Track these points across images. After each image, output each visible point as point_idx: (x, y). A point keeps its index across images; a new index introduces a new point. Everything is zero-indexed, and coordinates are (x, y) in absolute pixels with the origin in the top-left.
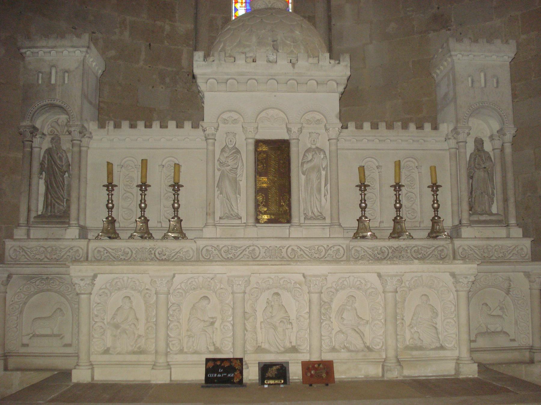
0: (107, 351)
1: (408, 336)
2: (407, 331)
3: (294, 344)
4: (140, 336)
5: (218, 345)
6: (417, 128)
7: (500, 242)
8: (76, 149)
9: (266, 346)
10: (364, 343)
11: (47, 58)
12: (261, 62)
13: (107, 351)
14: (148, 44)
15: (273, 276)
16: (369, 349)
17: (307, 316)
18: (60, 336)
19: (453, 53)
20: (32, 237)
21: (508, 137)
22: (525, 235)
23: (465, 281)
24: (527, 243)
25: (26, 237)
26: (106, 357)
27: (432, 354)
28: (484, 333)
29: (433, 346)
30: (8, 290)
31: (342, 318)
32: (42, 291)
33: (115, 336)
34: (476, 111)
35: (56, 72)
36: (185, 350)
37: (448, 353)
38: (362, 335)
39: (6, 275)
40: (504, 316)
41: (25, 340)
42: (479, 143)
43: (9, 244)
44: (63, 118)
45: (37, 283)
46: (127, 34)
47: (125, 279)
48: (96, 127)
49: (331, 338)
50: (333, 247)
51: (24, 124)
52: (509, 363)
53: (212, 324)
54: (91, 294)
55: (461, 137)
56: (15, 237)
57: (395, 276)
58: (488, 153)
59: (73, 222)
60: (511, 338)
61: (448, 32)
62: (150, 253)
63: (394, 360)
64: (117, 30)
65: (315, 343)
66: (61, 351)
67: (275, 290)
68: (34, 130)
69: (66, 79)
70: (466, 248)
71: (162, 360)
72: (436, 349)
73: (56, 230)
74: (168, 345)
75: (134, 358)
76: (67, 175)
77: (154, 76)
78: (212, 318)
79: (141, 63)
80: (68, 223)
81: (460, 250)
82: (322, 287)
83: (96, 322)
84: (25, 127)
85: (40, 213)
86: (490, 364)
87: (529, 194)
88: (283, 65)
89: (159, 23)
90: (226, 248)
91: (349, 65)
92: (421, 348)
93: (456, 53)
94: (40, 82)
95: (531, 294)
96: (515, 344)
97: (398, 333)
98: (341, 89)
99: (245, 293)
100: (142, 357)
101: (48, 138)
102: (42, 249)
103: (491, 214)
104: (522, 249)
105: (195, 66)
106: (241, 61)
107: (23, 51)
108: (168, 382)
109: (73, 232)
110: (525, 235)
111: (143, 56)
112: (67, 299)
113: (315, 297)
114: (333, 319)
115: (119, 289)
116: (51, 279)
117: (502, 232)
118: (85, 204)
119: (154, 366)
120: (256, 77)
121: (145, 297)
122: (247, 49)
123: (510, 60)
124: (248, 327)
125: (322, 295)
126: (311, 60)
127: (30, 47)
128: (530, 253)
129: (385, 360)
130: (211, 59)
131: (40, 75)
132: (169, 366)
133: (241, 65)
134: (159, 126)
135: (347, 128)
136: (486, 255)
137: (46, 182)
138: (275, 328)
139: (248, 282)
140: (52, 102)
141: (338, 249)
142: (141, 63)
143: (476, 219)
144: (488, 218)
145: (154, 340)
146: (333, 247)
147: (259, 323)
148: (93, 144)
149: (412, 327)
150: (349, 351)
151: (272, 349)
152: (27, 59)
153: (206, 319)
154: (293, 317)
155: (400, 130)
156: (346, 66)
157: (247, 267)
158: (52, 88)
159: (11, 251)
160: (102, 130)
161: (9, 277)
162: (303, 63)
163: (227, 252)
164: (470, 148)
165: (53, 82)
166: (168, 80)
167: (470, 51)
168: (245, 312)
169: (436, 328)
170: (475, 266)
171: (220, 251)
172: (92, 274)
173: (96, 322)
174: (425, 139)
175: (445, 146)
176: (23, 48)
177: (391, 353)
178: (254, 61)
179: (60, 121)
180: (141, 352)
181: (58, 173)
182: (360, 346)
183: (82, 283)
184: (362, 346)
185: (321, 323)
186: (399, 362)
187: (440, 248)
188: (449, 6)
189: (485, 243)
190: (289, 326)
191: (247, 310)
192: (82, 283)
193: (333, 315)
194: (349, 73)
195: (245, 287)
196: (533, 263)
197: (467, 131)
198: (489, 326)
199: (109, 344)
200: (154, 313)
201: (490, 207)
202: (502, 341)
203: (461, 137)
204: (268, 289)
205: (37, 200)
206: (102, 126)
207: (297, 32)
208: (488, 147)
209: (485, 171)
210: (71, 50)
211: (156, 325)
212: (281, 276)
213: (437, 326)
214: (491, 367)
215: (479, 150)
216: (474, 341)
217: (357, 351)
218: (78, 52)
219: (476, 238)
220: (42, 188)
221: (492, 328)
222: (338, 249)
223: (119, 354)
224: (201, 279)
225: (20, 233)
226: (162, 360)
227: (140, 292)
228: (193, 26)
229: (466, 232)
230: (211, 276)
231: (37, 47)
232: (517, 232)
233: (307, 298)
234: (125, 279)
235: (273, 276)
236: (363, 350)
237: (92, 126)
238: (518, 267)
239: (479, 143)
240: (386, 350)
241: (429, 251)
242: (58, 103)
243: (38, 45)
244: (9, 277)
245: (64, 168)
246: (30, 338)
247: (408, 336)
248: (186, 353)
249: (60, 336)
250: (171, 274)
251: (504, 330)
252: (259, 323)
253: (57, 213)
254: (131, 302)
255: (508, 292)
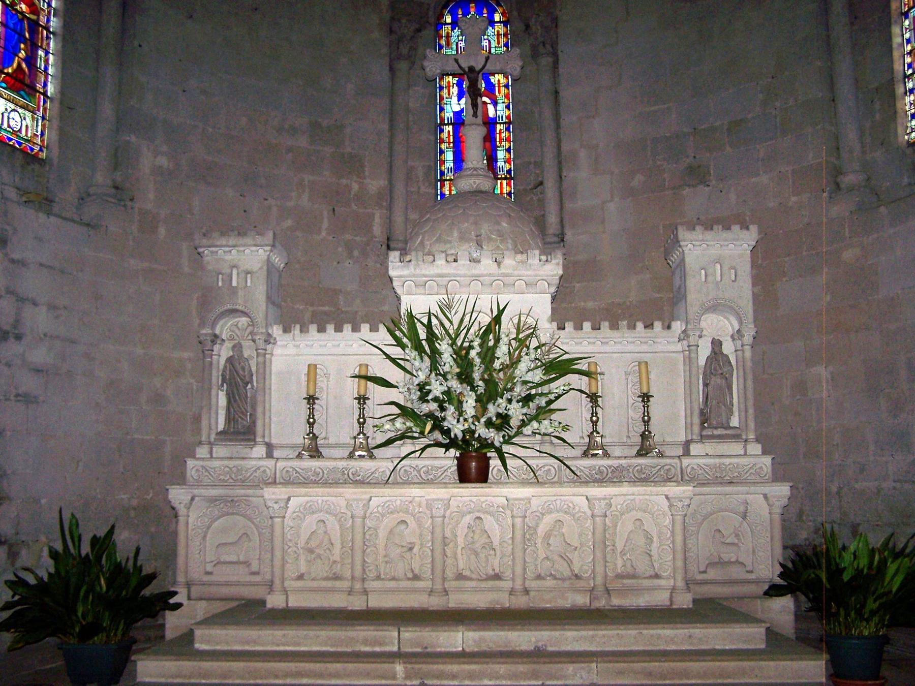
0: (301, 577)
1: (620, 563)
2: (619, 558)
3: (497, 571)
4: (335, 562)
5: (417, 571)
6: (645, 327)
7: (735, 460)
8: (261, 359)
9: (467, 573)
10: (572, 571)
11: (228, 257)
12: (463, 261)
13: (301, 577)
14: (331, 208)
15: (474, 499)
16: (577, 577)
17: (510, 542)
18: (247, 563)
19: (682, 243)
20: (214, 455)
21: (748, 338)
22: (765, 452)
23: (680, 505)
24: (767, 460)
25: (209, 456)
26: (300, 584)
27: (646, 583)
28: (716, 563)
29: (647, 575)
30: (191, 514)
31: (548, 544)
32: (228, 514)
33: (310, 561)
34: (714, 307)
35: (238, 274)
36: (383, 576)
37: (663, 582)
38: (569, 562)
39: (190, 498)
40: (740, 545)
41: (209, 568)
42: (717, 344)
43: (190, 463)
44: (244, 320)
45: (222, 506)
46: (305, 197)
47: (320, 502)
48: (281, 332)
49: (536, 565)
50: (543, 467)
51: (204, 332)
52: (741, 598)
53: (411, 549)
54: (284, 517)
55: (692, 340)
56: (197, 456)
57: (605, 499)
58: (727, 356)
59: (259, 439)
60: (748, 569)
61: (707, 189)
62: (343, 474)
63: (601, 588)
64: (294, 194)
65: (519, 570)
66: (248, 579)
67: (478, 514)
68: (215, 338)
69: (249, 281)
70: (695, 467)
71: (358, 586)
72: (651, 577)
73: (239, 449)
74: (364, 570)
75: (329, 584)
76: (249, 386)
77: (340, 249)
78: (411, 543)
79: (324, 233)
80: (254, 440)
81: (689, 470)
82: (526, 511)
83: (290, 547)
84: (206, 335)
85: (219, 430)
86: (726, 599)
87: (798, 397)
88: (487, 264)
89: (344, 181)
90: (425, 469)
91: (561, 263)
92: (634, 577)
93: (686, 243)
94: (220, 284)
95: (771, 520)
96: (752, 576)
97: (608, 559)
98: (553, 289)
99: (444, 517)
100: (338, 584)
101: (228, 345)
102: (227, 469)
103: (729, 428)
104: (761, 468)
105: (390, 268)
106: (441, 262)
107: (201, 250)
108: (365, 608)
109: (260, 451)
110: (765, 452)
111: (325, 224)
112: (253, 523)
113: (518, 521)
114: (539, 545)
115: (313, 513)
116: (236, 502)
117: (736, 448)
118: (270, 417)
119: (350, 592)
120: (458, 278)
121: (340, 520)
122: (448, 245)
123: (751, 248)
124: (449, 553)
125: (527, 520)
126: (519, 257)
127: (210, 247)
128: (770, 470)
129: (593, 589)
130: (408, 258)
131: (220, 276)
132: (365, 592)
133: (441, 266)
134: (350, 328)
135: (564, 329)
136: (719, 475)
137: (228, 394)
138: (477, 554)
139: (448, 506)
140: (235, 307)
141: (549, 470)
142: (324, 233)
143: (710, 433)
144: (724, 432)
145: (349, 566)
146: (543, 467)
147: (460, 548)
148: (278, 351)
149: (625, 554)
150: (555, 578)
151: (474, 576)
152: (207, 259)
153: (404, 544)
154: (496, 543)
155: (625, 330)
156: (558, 264)
157: (444, 490)
158: (234, 291)
159: (193, 473)
160: (287, 335)
161: (193, 499)
162: (509, 262)
163: (427, 472)
164: (704, 352)
165: (234, 284)
166: (356, 253)
167: (703, 240)
168: (444, 538)
169: (650, 556)
170: (691, 488)
171: (419, 471)
172: (286, 497)
173: (290, 547)
174: (655, 340)
175: (679, 347)
176: (201, 247)
177: (599, 580)
178: (455, 261)
179: (240, 325)
180: (337, 578)
181: (242, 385)
182: (567, 573)
183: (276, 506)
184: (570, 574)
185: (525, 550)
186: (608, 591)
187: (667, 467)
188: (708, 155)
189: (717, 461)
190: (492, 552)
191: (446, 535)
192: (276, 506)
193: (539, 541)
194: (561, 272)
195: (445, 511)
196: (774, 484)
197: (698, 333)
198: (722, 555)
199: (303, 569)
200: (350, 538)
201: (728, 419)
202: (736, 573)
203: (692, 340)
204: (470, 513)
205: (217, 414)
206: (286, 330)
207: (504, 224)
208: (728, 348)
209: (722, 378)
210: (254, 248)
211: (352, 550)
212: (483, 499)
213: (652, 553)
214: (721, 602)
215: (715, 353)
216: (705, 572)
217: (563, 580)
218: (261, 251)
219: (707, 455)
220: (223, 400)
221: (726, 558)
222: (549, 470)
223: (313, 580)
224: (398, 502)
225: (202, 452)
226: (358, 586)
227: (335, 515)
228: (386, 182)
229: (695, 449)
230: (410, 499)
231: (216, 246)
232: (755, 448)
233: (510, 521)
234: (320, 502)
235: (474, 499)
236: (570, 579)
237: (276, 331)
238: (753, 489)
239: (717, 344)
240: (594, 578)
241: (654, 470)
242: (240, 308)
243: (218, 243)
244: (193, 499)
245: (247, 379)
246: (215, 566)
247: (620, 563)
248: (383, 579)
249: (247, 563)
250: (368, 497)
251: (741, 560)
252: (460, 548)
253: (242, 428)
254: (325, 527)
255: (744, 517)
